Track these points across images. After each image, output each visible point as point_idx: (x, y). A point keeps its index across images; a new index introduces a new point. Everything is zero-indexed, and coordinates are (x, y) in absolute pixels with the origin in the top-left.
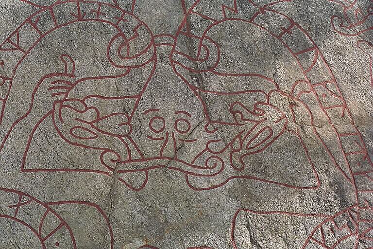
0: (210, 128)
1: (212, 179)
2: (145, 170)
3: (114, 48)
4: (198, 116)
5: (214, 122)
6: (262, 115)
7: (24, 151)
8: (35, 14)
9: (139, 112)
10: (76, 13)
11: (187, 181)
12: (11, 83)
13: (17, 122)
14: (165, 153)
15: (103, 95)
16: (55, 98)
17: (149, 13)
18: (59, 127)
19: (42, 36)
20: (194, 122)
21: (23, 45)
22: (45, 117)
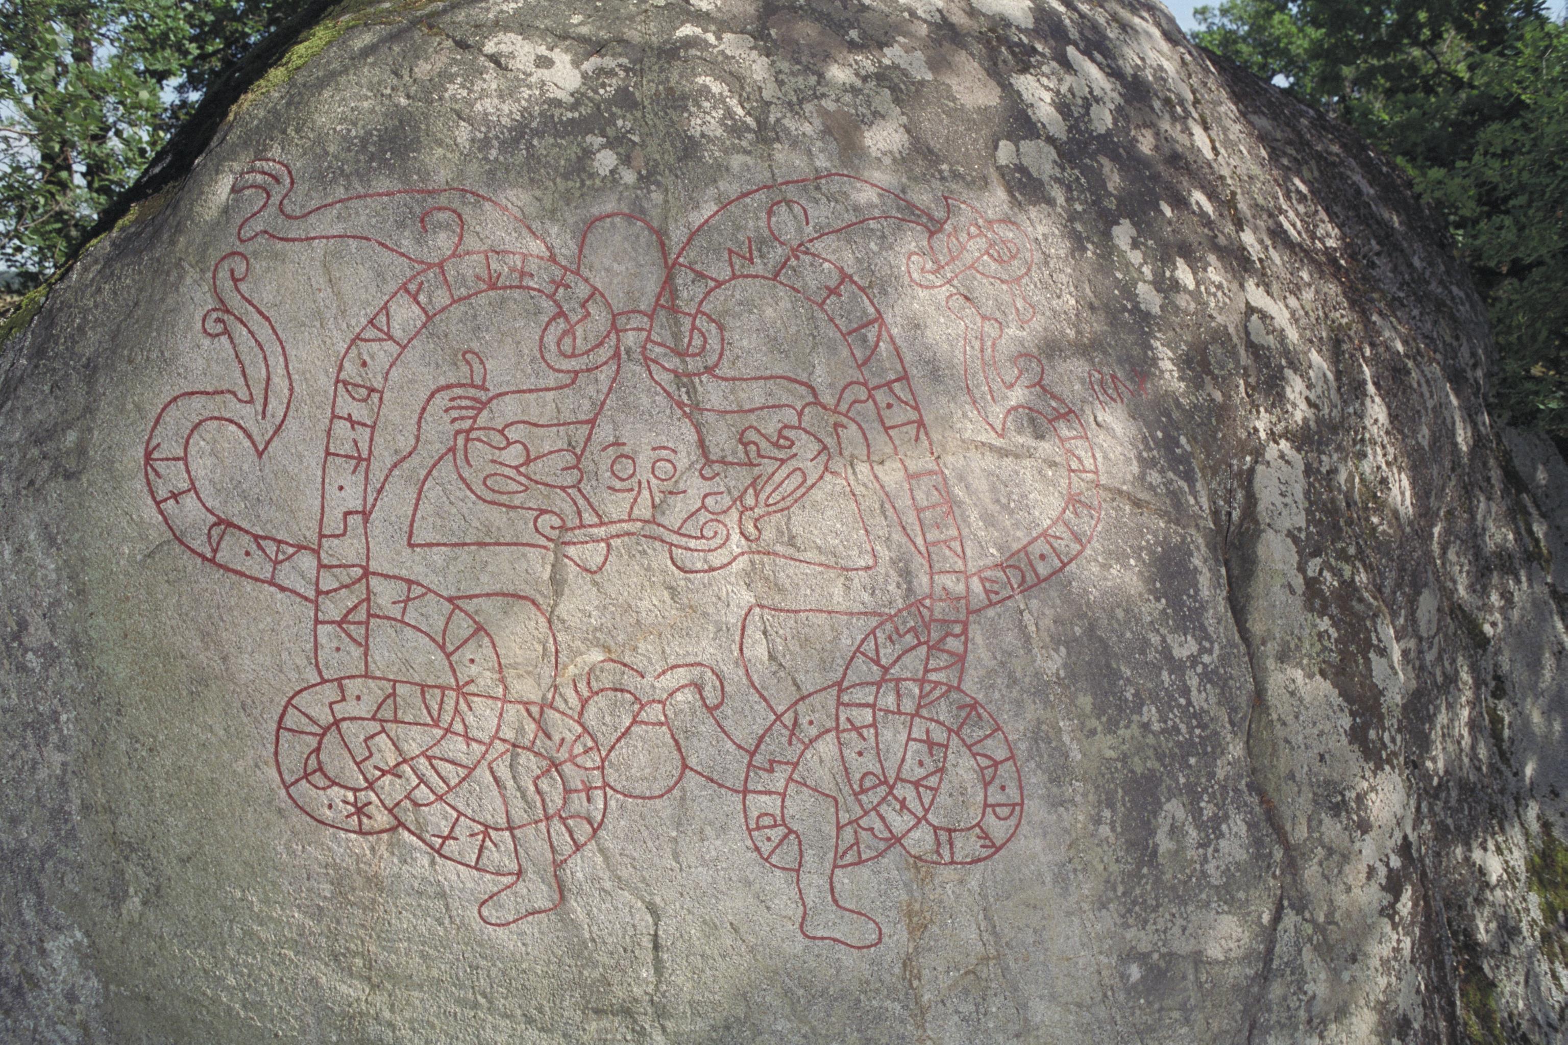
0: (707, 472)
1: (710, 556)
2: (606, 541)
3: (550, 339)
4: (689, 454)
5: (713, 462)
6: (790, 447)
7: (410, 513)
8: (414, 277)
9: (594, 447)
10: (486, 277)
11: (672, 558)
12: (381, 399)
13: (395, 466)
14: (636, 512)
15: (534, 420)
16: (457, 426)
17: (607, 270)
18: (466, 475)
19: (429, 318)
20: (682, 461)
21: (397, 333)
22: (441, 458)
